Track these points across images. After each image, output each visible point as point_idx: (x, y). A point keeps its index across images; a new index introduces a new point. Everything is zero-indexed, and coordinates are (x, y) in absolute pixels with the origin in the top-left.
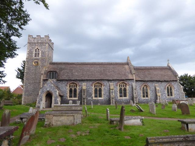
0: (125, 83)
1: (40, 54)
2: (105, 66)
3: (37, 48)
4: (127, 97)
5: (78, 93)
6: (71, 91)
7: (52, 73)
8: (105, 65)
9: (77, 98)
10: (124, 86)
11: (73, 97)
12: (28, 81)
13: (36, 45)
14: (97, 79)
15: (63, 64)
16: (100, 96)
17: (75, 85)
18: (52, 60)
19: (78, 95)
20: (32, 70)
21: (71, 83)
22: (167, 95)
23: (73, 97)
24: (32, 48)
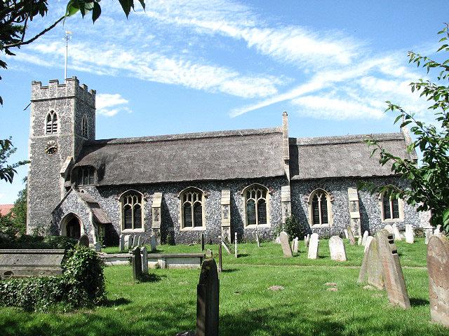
0: (260, 187)
2: (245, 142)
3: (52, 112)
4: (268, 225)
5: (143, 216)
7: (83, 170)
8: (220, 140)
10: (195, 199)
11: (320, 222)
12: (36, 191)
13: (48, 106)
14: (223, 178)
16: (198, 223)
17: (261, 191)
18: (93, 134)
20: (44, 165)
21: (188, 191)
22: (382, 216)
23: (320, 222)
24: (42, 112)
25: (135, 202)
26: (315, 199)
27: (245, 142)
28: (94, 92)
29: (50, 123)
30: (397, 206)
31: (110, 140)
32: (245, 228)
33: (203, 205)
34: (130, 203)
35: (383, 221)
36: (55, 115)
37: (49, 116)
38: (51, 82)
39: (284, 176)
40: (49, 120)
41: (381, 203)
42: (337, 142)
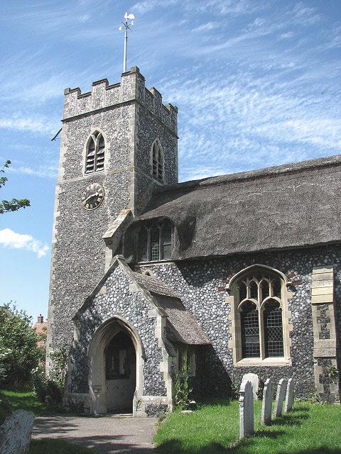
1: (107, 156)
6: (245, 315)
9: (284, 360)
15: (215, 184)
19: (287, 342)
25: (265, 294)
34: (254, 295)
36: (101, 140)
37: (91, 142)
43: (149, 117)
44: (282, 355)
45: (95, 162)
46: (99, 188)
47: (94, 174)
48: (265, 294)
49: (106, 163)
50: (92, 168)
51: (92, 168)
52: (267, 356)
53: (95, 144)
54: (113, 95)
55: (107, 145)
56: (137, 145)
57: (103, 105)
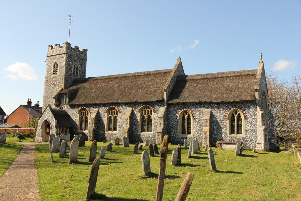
4: (243, 135)
18: (85, 75)
25: (148, 114)
26: (233, 116)
27: (152, 78)
28: (85, 51)
29: (55, 69)
30: (241, 125)
31: (94, 77)
32: (106, 132)
33: (153, 118)
34: (145, 114)
35: (228, 135)
36: (57, 64)
37: (54, 65)
38: (56, 45)
39: (163, 100)
40: (54, 67)
41: (228, 122)
42: (236, 74)
43: (73, 57)
44: (183, 145)
45: (55, 72)
46: (55, 80)
47: (55, 75)
48: (148, 114)
49: (58, 72)
50: (54, 73)
51: (54, 73)
52: (114, 131)
53: (56, 66)
54: (60, 50)
55: (58, 67)
56: (66, 68)
57: (58, 53)
